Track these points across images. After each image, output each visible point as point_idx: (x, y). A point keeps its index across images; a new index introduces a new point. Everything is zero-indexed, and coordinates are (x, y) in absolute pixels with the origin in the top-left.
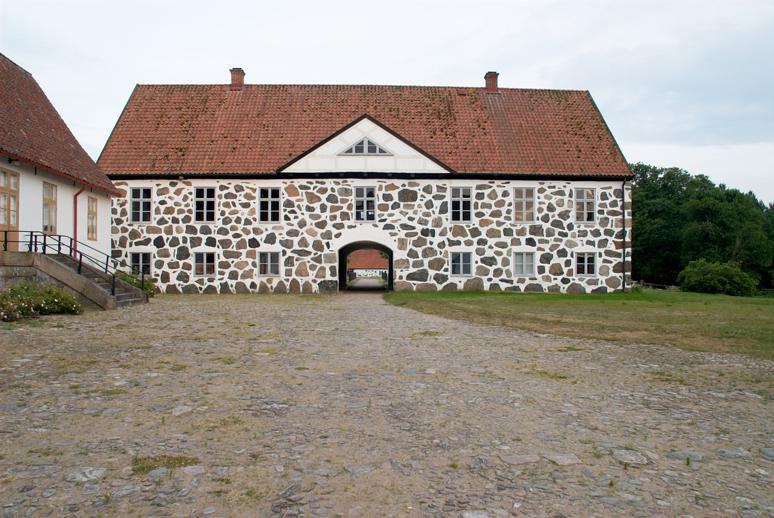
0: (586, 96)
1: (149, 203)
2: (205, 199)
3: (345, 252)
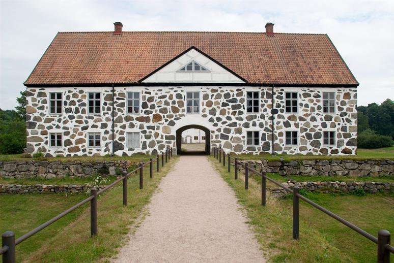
0: (324, 41)
1: (258, 101)
2: (291, 99)
3: (179, 132)
